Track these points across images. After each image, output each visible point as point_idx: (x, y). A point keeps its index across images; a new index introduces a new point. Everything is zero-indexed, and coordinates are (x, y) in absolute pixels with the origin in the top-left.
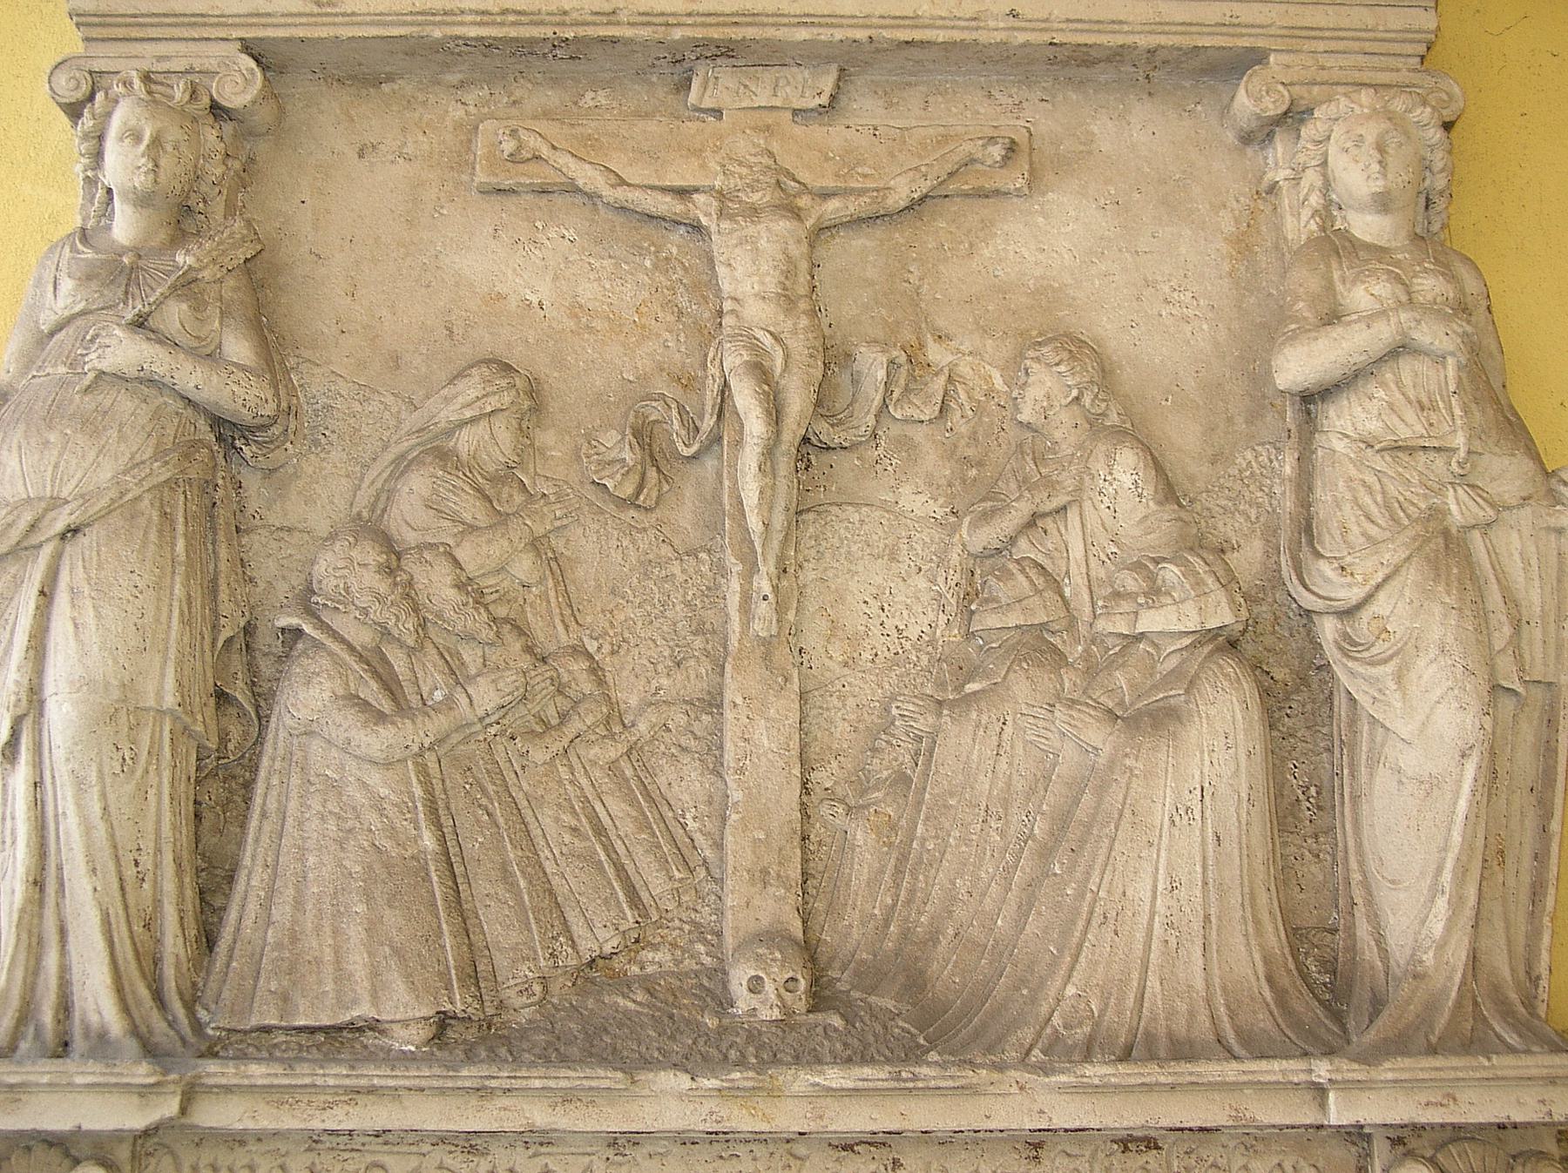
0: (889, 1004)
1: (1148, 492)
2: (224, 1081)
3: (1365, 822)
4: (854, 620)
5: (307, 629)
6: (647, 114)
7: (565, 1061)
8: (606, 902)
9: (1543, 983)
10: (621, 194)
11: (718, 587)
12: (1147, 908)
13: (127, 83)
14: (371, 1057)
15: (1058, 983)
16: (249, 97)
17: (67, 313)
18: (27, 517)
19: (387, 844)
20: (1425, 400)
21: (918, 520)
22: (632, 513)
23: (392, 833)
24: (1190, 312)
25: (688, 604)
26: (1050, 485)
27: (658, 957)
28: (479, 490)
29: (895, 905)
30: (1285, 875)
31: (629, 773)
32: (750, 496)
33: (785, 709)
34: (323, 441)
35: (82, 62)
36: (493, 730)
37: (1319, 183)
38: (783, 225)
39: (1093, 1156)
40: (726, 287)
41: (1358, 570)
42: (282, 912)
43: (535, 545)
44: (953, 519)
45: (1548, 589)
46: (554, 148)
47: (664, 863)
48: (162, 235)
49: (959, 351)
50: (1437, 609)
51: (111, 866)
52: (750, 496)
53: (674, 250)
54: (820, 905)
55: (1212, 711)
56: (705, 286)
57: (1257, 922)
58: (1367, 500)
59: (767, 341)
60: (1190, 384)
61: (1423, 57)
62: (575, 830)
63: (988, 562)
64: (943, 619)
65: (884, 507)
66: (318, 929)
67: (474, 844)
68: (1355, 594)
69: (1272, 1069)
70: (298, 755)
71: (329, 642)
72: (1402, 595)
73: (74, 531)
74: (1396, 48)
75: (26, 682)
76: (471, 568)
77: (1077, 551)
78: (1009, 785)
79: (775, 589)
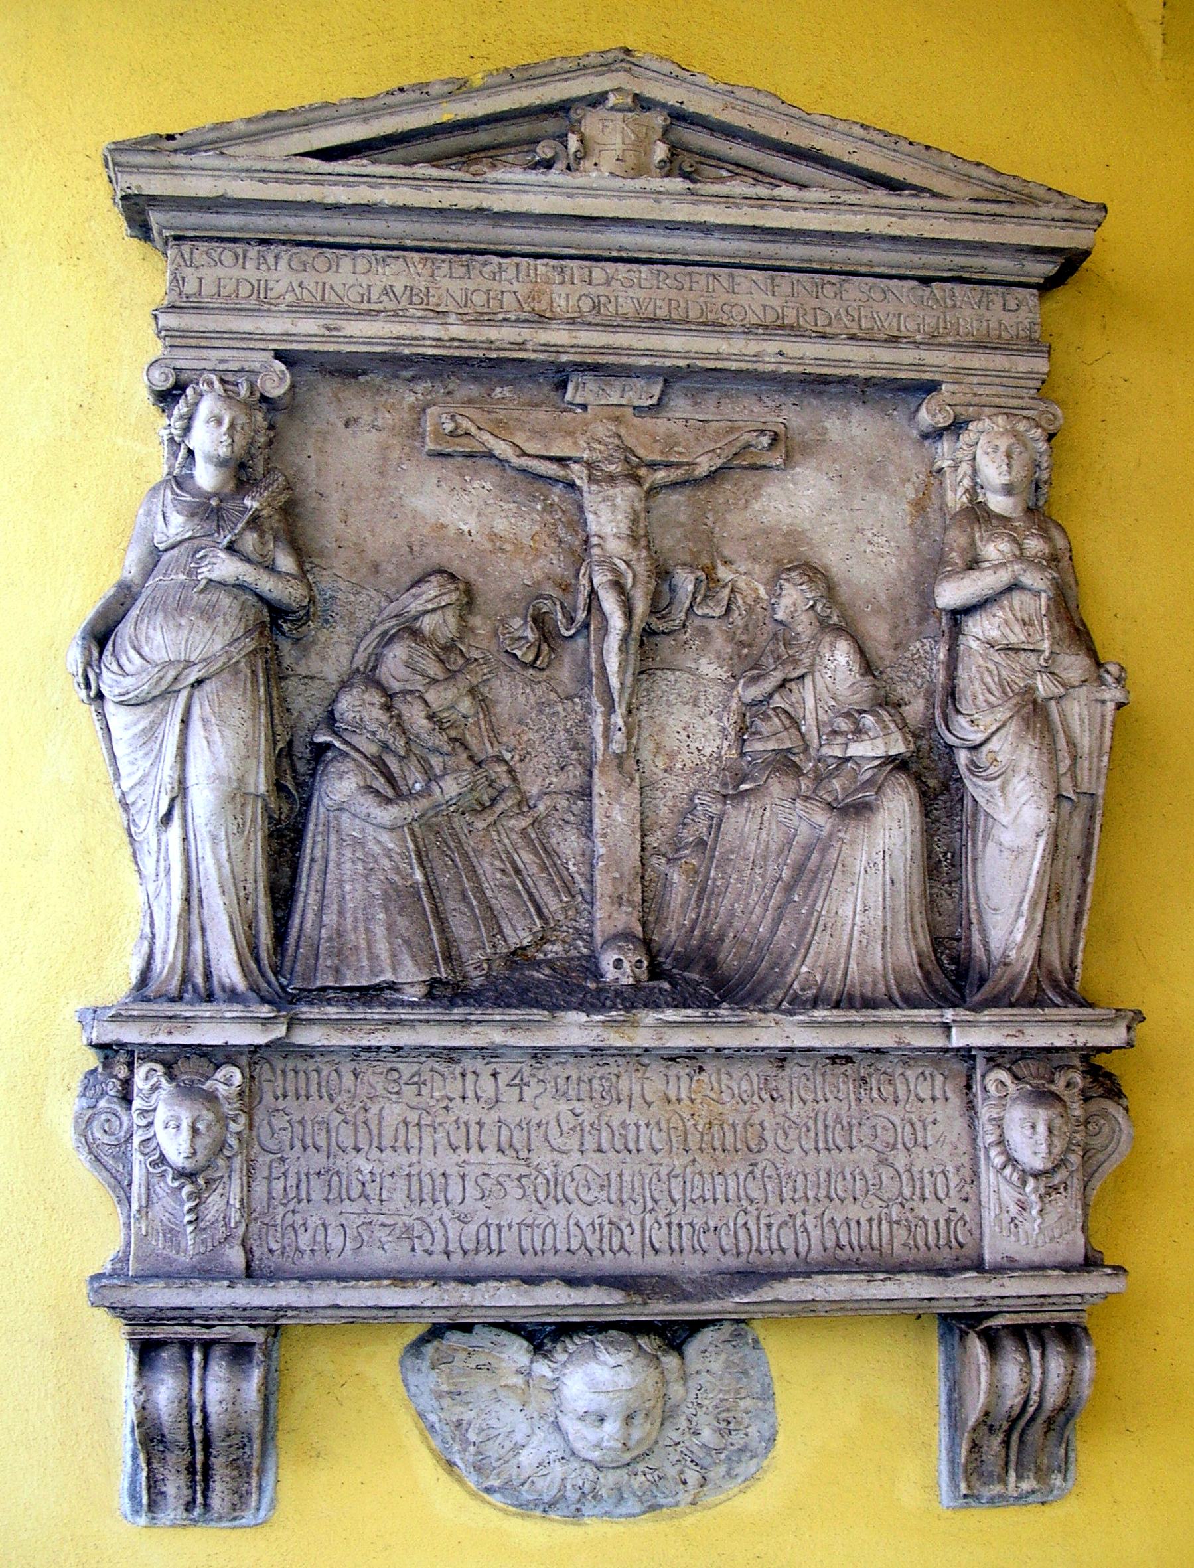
0: (696, 976)
1: (856, 668)
2: (312, 1017)
3: (980, 874)
4: (671, 744)
5: (337, 744)
6: (537, 405)
7: (509, 1006)
8: (524, 914)
9: (1078, 970)
10: (524, 462)
11: (586, 720)
12: (850, 922)
13: (210, 383)
14: (390, 1004)
15: (797, 965)
16: (283, 391)
17: (179, 538)
18: (172, 673)
19: (396, 878)
20: (1027, 619)
21: (711, 680)
22: (531, 671)
23: (398, 870)
24: (885, 550)
25: (567, 731)
26: (795, 661)
27: (555, 948)
28: (437, 656)
29: (697, 919)
30: (931, 905)
31: (533, 836)
32: (613, 665)
33: (631, 798)
34: (331, 620)
35: (167, 361)
36: (452, 809)
37: (970, 472)
38: (631, 489)
39: (815, 1066)
40: (593, 527)
41: (981, 723)
42: (330, 919)
43: (472, 691)
44: (732, 680)
45: (1094, 737)
46: (479, 428)
47: (557, 892)
48: (231, 485)
49: (737, 571)
50: (1027, 749)
51: (233, 890)
52: (613, 665)
53: (556, 499)
54: (651, 919)
55: (891, 805)
56: (578, 520)
57: (914, 932)
58: (989, 680)
59: (623, 566)
60: (883, 597)
61: (1039, 390)
62: (503, 871)
63: (754, 708)
64: (726, 744)
65: (689, 671)
66: (355, 929)
67: (445, 879)
68: (980, 737)
69: (921, 1014)
70: (333, 823)
71: (352, 753)
72: (1006, 739)
73: (199, 682)
74: (1022, 383)
75: (176, 777)
76: (435, 706)
77: (810, 704)
78: (767, 847)
79: (625, 723)
